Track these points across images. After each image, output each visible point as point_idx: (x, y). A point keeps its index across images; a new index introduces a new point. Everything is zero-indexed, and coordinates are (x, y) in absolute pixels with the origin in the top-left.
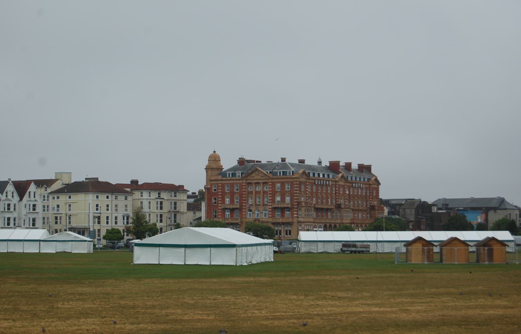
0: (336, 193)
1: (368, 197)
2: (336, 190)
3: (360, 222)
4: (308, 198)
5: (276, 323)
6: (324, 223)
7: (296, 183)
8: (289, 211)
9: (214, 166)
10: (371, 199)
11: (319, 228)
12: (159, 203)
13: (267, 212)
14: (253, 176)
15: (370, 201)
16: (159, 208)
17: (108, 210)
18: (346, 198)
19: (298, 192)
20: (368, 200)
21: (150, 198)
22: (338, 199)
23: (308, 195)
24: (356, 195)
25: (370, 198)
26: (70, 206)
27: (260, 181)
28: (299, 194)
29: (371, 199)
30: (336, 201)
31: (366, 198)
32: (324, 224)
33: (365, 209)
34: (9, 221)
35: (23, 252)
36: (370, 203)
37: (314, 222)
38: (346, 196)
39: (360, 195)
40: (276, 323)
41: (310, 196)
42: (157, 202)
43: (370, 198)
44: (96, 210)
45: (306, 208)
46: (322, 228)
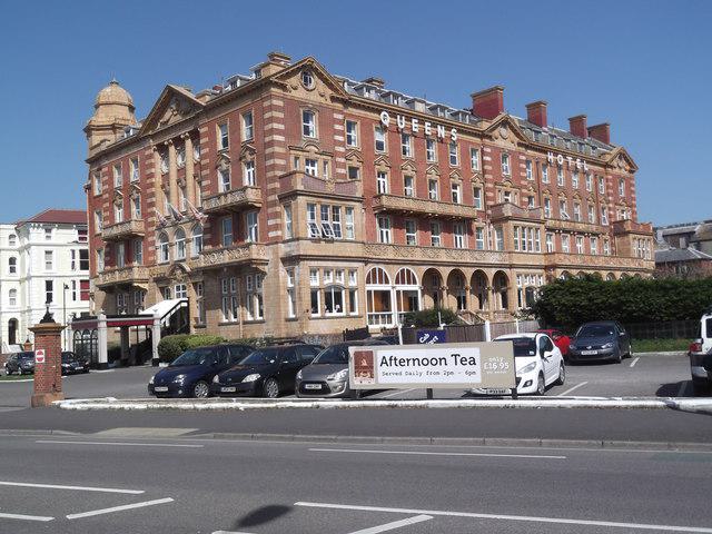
0: (484, 172)
4: (526, 200)
5: (333, 437)
9: (104, 120)
10: (611, 205)
11: (397, 282)
12: (77, 254)
15: (610, 209)
16: (78, 265)
17: (12, 270)
18: (524, 191)
20: (603, 209)
21: (49, 242)
23: (524, 191)
24: (564, 191)
25: (608, 202)
26: (48, 253)
28: (496, 184)
29: (611, 205)
31: (597, 201)
32: (425, 268)
34: (338, 212)
36: (610, 216)
37: (366, 261)
38: (525, 187)
40: (333, 437)
41: (533, 193)
42: (73, 251)
43: (608, 202)
44: (47, 268)
46: (415, 282)
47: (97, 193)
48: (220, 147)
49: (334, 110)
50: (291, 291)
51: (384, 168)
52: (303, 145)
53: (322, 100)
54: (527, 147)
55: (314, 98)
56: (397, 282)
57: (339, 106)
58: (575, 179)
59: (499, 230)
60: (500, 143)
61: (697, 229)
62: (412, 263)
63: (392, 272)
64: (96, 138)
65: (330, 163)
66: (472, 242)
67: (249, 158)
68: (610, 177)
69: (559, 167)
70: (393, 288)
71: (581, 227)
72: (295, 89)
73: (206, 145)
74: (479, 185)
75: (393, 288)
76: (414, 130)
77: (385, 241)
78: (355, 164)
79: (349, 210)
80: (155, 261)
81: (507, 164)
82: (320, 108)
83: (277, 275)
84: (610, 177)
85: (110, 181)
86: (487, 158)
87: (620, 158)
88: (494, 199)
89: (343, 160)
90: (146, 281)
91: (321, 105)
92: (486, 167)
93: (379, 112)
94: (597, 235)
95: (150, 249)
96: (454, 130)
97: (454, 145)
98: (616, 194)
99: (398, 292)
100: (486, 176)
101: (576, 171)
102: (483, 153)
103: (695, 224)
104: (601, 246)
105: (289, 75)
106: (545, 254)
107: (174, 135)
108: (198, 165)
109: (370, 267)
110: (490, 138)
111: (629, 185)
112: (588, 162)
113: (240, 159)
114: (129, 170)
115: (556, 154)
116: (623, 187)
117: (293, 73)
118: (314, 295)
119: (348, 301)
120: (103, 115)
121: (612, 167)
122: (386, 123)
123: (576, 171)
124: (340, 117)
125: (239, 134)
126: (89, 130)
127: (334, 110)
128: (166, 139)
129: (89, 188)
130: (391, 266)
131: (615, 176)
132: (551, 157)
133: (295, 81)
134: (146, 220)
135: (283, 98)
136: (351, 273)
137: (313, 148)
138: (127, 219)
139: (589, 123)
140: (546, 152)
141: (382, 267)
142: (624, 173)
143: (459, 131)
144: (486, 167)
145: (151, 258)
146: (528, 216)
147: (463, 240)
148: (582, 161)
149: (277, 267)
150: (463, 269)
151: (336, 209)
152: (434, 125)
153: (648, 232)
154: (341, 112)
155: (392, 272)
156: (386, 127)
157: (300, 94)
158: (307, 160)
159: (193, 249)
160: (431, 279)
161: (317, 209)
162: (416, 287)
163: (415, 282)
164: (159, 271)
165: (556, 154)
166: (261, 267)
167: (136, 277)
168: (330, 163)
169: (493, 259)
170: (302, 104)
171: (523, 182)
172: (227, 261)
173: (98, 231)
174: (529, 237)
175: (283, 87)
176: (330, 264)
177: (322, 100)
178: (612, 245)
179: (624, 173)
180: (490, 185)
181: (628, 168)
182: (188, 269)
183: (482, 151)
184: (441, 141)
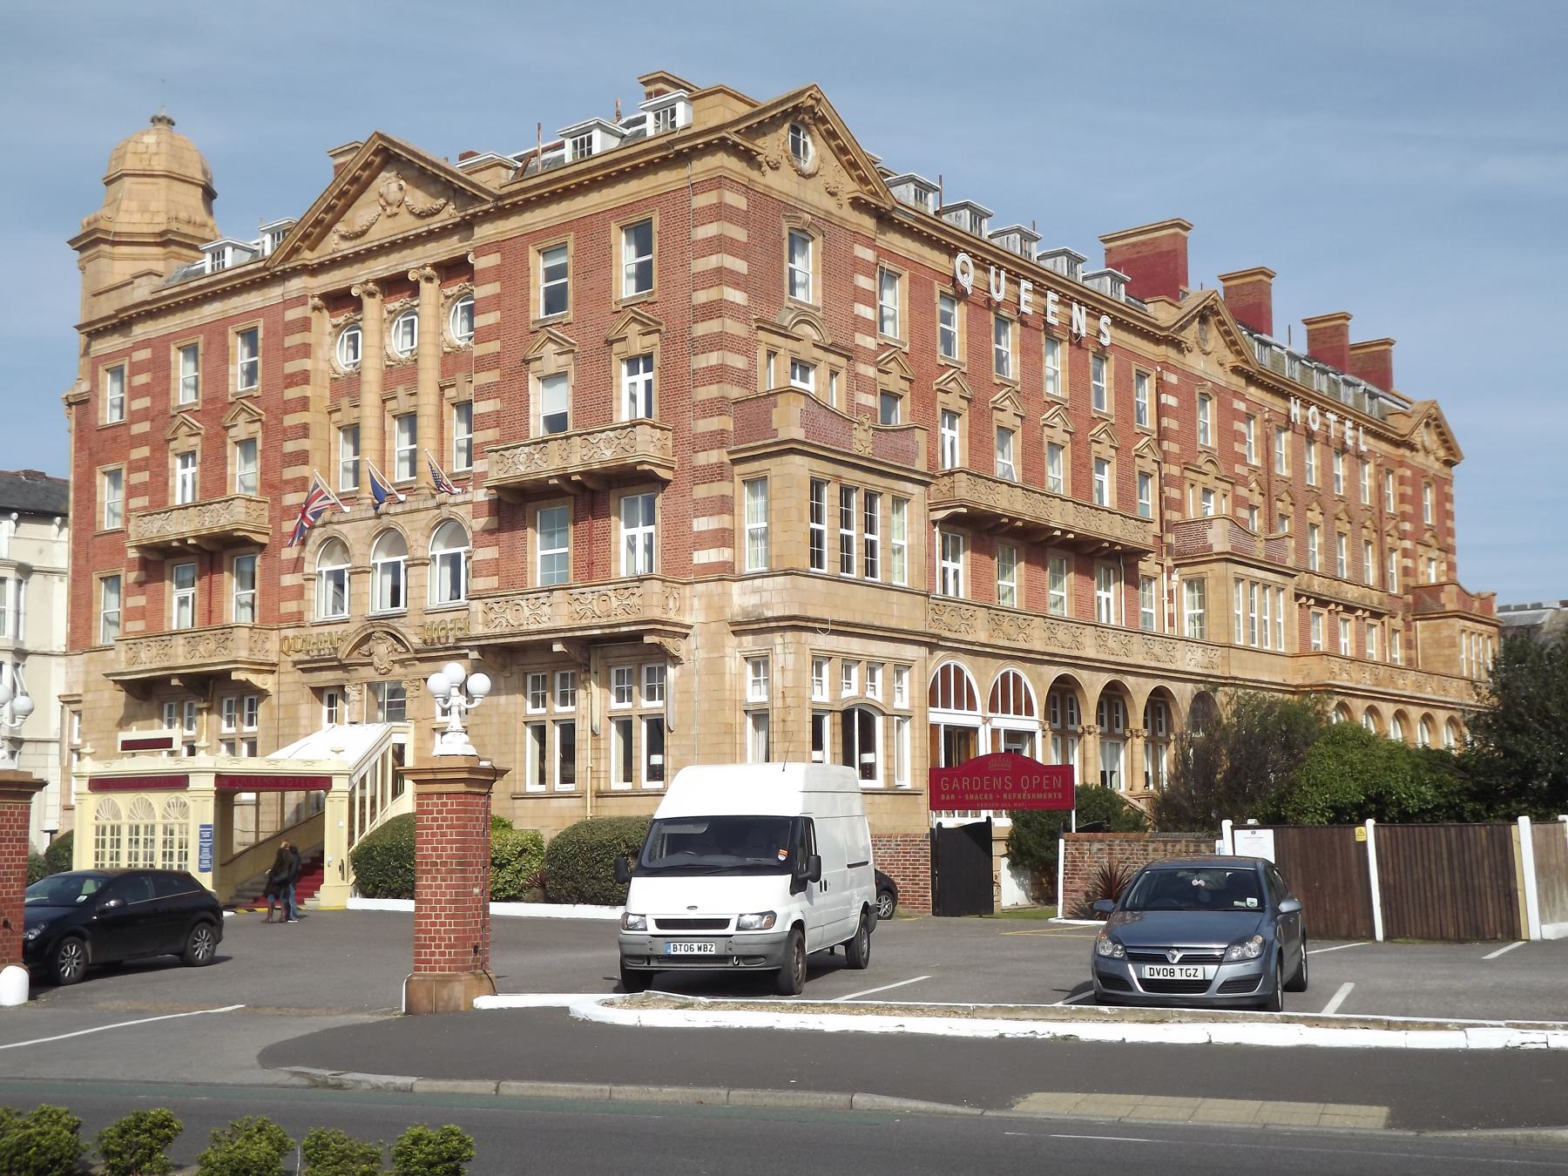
0: (1162, 434)
1: (1389, 527)
2: (1161, 410)
3: (1365, 681)
6: (1049, 659)
7: (702, 200)
8: (650, 521)
9: (137, 217)
11: (993, 708)
13: (461, 550)
14: (357, 229)
18: (1242, 491)
19: (737, 296)
22: (1178, 483)
23: (1242, 491)
24: (1316, 495)
27: (411, 261)
30: (1165, 503)
32: (1054, 672)
33: (1375, 598)
35: (1085, 783)
36: (1406, 571)
38: (1244, 482)
39: (1341, 499)
45: (824, 469)
47: (109, 416)
48: (538, 311)
49: (857, 237)
50: (760, 717)
51: (954, 402)
52: (787, 319)
53: (830, 204)
54: (1250, 379)
55: (813, 196)
56: (993, 708)
57: (868, 223)
58: (1340, 468)
59: (1197, 584)
60: (1196, 363)
61: (1546, 617)
62: (976, 651)
63: (981, 677)
64: (118, 266)
65: (843, 374)
66: (1132, 609)
67: (638, 343)
68: (1408, 473)
69: (1310, 437)
70: (986, 720)
71: (1351, 593)
72: (775, 168)
73: (495, 302)
74: (1150, 467)
75: (986, 720)
76: (1024, 308)
77: (951, 593)
78: (894, 383)
79: (899, 501)
80: (301, 613)
81: (1208, 416)
82: (826, 225)
83: (715, 668)
84: (1408, 473)
85: (161, 385)
86: (1170, 400)
87: (1427, 425)
88: (1180, 505)
89: (871, 371)
90: (271, 668)
91: (828, 219)
92: (1165, 422)
93: (952, 252)
94: (1376, 615)
95: (288, 580)
96: (1105, 319)
97: (1101, 355)
98: (1417, 517)
99: (995, 732)
100: (1166, 445)
101: (1343, 450)
102: (1161, 386)
103: (1538, 606)
104: (1386, 643)
105: (761, 129)
106: (251, 628)
107: (382, 267)
108: (452, 361)
109: (941, 659)
110: (1177, 345)
111: (1444, 498)
112: (1368, 432)
113: (610, 343)
114: (225, 357)
115: (1306, 405)
116: (1429, 497)
117: (771, 125)
118: (817, 722)
119: (839, 739)
120: (134, 205)
121: (1412, 448)
122: (967, 281)
123: (1343, 450)
124: (868, 255)
125: (608, 280)
126: (89, 242)
127: (857, 237)
128: (356, 277)
129: (82, 404)
130: (981, 660)
131: (1420, 473)
132: (1296, 410)
133: (774, 145)
134: (277, 500)
135: (747, 189)
136: (901, 668)
137: (808, 330)
138: (213, 487)
139: (1357, 334)
140: (1286, 397)
141: (964, 663)
142: (1435, 467)
143: (1117, 323)
144: (1165, 422)
145: (289, 607)
146: (1262, 557)
147: (1110, 597)
148: (1356, 428)
149: (716, 646)
150: (1130, 682)
151: (870, 498)
152: (1065, 302)
153: (1476, 611)
154: (870, 243)
155: (981, 677)
156: (964, 292)
157: (781, 182)
158: (795, 363)
159: (433, 587)
160: (1063, 696)
161: (830, 495)
162: (1030, 723)
163: (1030, 712)
164: (317, 640)
165: (1306, 405)
166: (669, 644)
167: (243, 654)
168: (843, 374)
169: (1191, 660)
170: (788, 208)
171: (1239, 469)
172: (561, 622)
173: (108, 523)
174: (1263, 610)
175: (749, 157)
176: (855, 646)
177: (830, 204)
178: (1409, 644)
179: (1435, 467)
180: (1175, 470)
181: (1442, 453)
182: (415, 640)
183: (1159, 379)
184: (1077, 342)
